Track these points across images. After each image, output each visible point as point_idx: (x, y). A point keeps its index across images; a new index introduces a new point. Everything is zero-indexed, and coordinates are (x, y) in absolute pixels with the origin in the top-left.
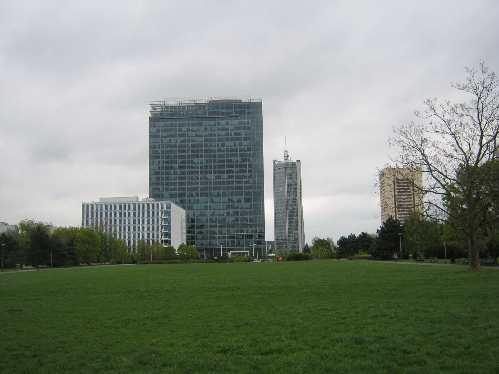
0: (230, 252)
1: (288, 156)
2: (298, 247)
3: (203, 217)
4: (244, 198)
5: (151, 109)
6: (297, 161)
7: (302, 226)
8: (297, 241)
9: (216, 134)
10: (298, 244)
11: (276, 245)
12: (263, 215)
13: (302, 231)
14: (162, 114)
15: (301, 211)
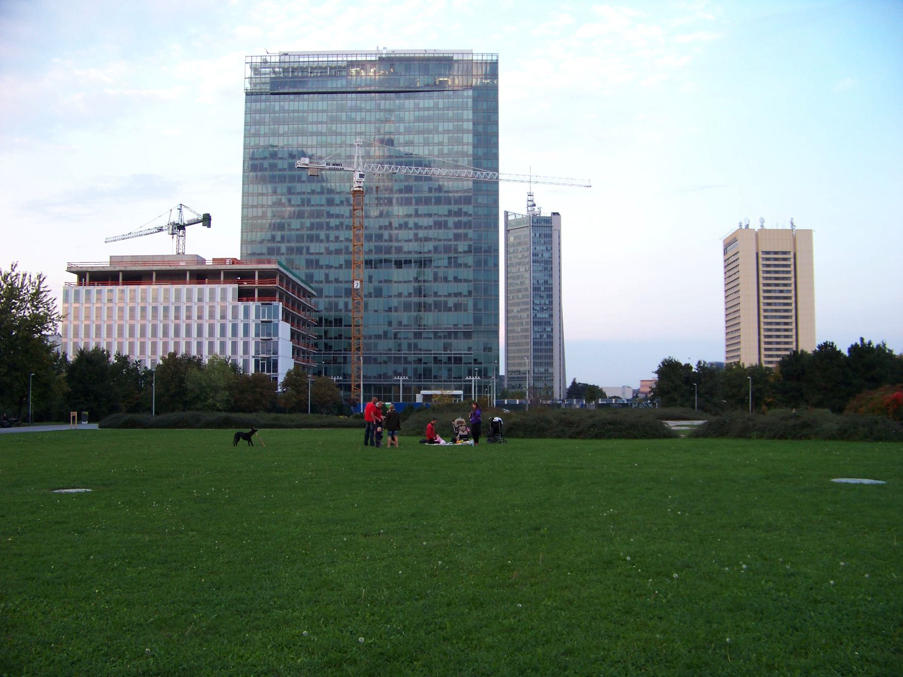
0: (420, 393)
1: (534, 205)
2: (552, 350)
3: (370, 299)
4: (444, 344)
5: (249, 73)
6: (554, 214)
8: (551, 361)
9: (371, 336)
12: (494, 150)
14: (274, 82)
15: (560, 314)
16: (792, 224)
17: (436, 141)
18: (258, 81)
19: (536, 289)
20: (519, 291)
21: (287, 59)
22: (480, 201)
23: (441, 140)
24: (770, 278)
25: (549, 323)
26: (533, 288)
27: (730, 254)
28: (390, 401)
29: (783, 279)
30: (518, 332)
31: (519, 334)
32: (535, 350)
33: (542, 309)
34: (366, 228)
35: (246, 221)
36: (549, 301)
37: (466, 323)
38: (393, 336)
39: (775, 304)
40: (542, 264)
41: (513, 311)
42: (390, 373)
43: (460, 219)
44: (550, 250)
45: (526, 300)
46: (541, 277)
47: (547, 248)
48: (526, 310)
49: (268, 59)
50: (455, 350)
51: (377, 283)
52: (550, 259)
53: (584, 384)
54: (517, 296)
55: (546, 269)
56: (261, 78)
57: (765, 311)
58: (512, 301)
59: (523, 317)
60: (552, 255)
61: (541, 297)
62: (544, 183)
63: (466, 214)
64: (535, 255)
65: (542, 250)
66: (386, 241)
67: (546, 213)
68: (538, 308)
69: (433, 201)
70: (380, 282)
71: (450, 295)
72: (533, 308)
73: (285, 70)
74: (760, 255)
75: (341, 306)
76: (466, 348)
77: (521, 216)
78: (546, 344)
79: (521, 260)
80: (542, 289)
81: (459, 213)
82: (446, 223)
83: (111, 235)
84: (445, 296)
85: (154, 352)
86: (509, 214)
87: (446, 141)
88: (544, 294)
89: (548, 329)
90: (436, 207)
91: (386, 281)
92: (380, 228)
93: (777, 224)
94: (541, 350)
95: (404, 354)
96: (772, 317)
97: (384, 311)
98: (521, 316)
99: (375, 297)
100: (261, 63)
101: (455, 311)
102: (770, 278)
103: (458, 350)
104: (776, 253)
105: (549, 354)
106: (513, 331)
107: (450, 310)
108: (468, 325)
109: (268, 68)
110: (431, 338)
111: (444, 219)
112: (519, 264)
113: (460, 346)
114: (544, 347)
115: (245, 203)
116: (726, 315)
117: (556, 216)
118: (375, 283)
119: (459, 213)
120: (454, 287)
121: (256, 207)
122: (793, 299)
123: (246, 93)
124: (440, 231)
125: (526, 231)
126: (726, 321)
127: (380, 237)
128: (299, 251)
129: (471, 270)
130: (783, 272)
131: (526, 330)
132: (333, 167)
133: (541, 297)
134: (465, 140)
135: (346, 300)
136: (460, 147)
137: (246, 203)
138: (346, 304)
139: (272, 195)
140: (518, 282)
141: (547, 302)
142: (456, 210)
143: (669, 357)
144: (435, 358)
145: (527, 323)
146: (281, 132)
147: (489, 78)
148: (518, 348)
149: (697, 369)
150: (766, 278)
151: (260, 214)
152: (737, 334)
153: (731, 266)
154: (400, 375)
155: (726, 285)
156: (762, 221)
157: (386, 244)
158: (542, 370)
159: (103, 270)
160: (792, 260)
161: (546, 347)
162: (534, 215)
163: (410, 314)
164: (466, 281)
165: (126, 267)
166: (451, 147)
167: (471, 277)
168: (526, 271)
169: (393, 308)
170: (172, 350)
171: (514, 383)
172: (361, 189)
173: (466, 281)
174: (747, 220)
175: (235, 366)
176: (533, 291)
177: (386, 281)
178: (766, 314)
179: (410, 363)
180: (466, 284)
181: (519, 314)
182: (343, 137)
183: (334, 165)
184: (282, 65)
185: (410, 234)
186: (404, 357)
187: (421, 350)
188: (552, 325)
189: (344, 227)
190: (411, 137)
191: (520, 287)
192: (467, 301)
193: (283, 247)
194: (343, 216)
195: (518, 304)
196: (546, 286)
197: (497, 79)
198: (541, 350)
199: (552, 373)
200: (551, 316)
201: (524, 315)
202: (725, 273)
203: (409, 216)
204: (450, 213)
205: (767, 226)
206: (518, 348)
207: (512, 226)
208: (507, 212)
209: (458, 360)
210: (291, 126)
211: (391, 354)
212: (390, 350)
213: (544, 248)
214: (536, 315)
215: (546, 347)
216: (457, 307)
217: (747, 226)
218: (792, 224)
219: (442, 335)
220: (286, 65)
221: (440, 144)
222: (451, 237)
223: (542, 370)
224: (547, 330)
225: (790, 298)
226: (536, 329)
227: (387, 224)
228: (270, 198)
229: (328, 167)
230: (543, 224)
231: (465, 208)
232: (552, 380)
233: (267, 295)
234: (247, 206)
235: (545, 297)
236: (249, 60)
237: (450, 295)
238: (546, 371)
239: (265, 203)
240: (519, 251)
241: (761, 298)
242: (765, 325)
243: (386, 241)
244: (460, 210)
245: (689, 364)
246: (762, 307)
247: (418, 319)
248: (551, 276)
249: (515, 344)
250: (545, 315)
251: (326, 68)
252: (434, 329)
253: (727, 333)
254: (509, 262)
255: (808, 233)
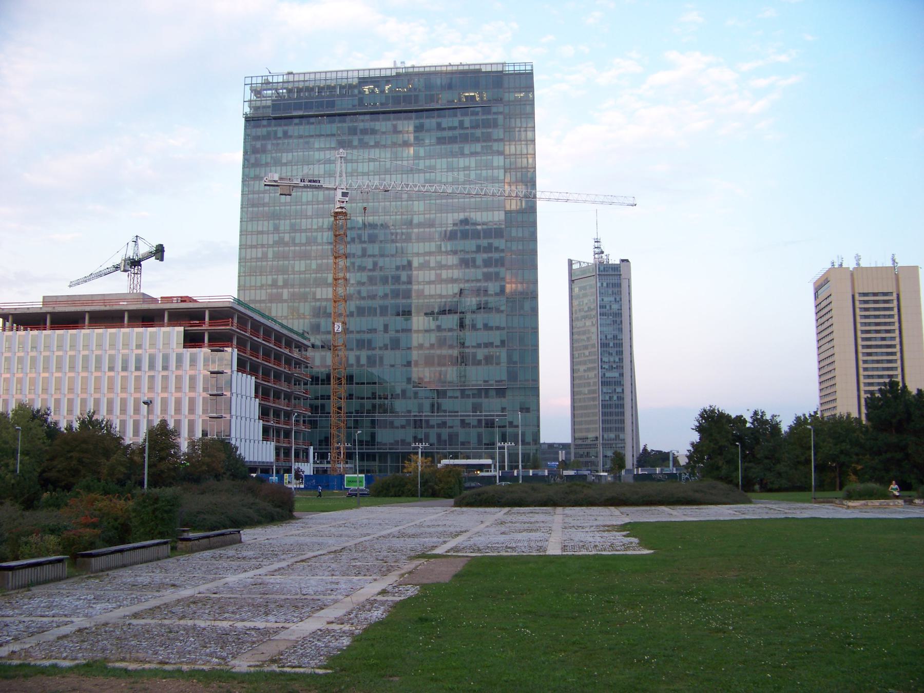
1: (602, 252)
2: (623, 414)
4: (473, 404)
5: (249, 95)
6: (623, 261)
7: (632, 407)
8: (622, 410)
10: (624, 416)
11: (575, 449)
13: (634, 428)
14: (275, 106)
16: (894, 261)
17: (461, 165)
18: (258, 104)
19: (604, 345)
20: (586, 347)
21: (291, 78)
22: (514, 234)
23: (467, 164)
24: (869, 324)
25: (620, 383)
26: (601, 344)
27: (821, 298)
28: (364, 473)
29: (885, 324)
30: (585, 394)
31: (586, 396)
32: (604, 414)
33: (612, 368)
34: (381, 269)
35: (243, 264)
36: (619, 359)
37: (498, 379)
38: (412, 395)
39: (876, 354)
40: (610, 317)
41: (579, 370)
42: (410, 439)
43: (490, 255)
44: (618, 301)
45: (593, 357)
46: (610, 331)
47: (615, 299)
48: (594, 368)
49: (270, 79)
50: (486, 411)
51: (393, 333)
52: (620, 311)
53: (657, 451)
54: (584, 354)
55: (615, 322)
56: (261, 100)
57: (865, 362)
58: (577, 360)
59: (590, 376)
60: (621, 306)
61: (611, 354)
62: (576, 201)
63: (497, 249)
64: (602, 307)
65: (611, 302)
66: (404, 283)
67: (615, 260)
68: (606, 366)
69: (459, 235)
70: (397, 331)
71: (479, 346)
72: (602, 367)
73: (290, 91)
74: (857, 297)
75: (352, 360)
76: (500, 409)
77: (586, 264)
78: (617, 406)
79: (588, 313)
80: (611, 344)
81: (489, 249)
82: (474, 260)
83: (74, 279)
84: (473, 347)
85: (70, 411)
86: (573, 262)
87: (473, 165)
88: (613, 351)
89: (619, 390)
90: (462, 242)
91: (403, 331)
92: (398, 268)
93: (876, 262)
94: (611, 414)
95: (426, 416)
96: (873, 369)
97: (402, 365)
98: (588, 375)
99: (392, 349)
100: (262, 84)
101: (487, 364)
102: (869, 324)
103: (489, 411)
104: (875, 294)
105: (619, 418)
106: (580, 393)
107: (479, 363)
108: (501, 381)
109: (269, 90)
110: (457, 397)
111: (472, 256)
112: (585, 317)
113: (492, 406)
114: (613, 410)
115: (242, 243)
116: (820, 369)
117: (625, 263)
118: (392, 333)
119: (489, 249)
120: (484, 336)
121: (256, 247)
122: (898, 347)
123: (246, 118)
124: (467, 270)
125: (592, 281)
126: (820, 383)
127: (397, 279)
128: (303, 298)
129: (504, 316)
130: (885, 316)
131: (594, 392)
132: (309, 184)
133: (611, 354)
134: (495, 164)
135: (358, 353)
136: (490, 172)
137: (245, 243)
138: (358, 359)
139: (273, 233)
140: (584, 337)
141: (617, 360)
142: (486, 245)
143: (711, 407)
144: (463, 421)
145: (595, 383)
146: (284, 161)
147: (524, 92)
148: (585, 412)
149: (752, 423)
150: (865, 324)
151: (260, 255)
152: (832, 390)
153: (823, 311)
154: (421, 441)
155: (818, 333)
156: (858, 258)
157: (404, 287)
158: (612, 435)
159: (30, 311)
160: (895, 302)
161: (617, 410)
162: (600, 262)
163: (432, 369)
164: (498, 328)
165: (54, 307)
166: (479, 172)
167: (503, 325)
168: (593, 325)
169: (413, 363)
170: (91, 407)
171: (581, 451)
172: (344, 210)
173: (498, 328)
174: (840, 258)
175: (109, 426)
176: (601, 347)
177: (403, 331)
178: (866, 366)
179: (433, 427)
180: (498, 332)
181: (586, 374)
182: (354, 165)
183: (310, 181)
184: (286, 85)
185: (432, 275)
186: (425, 420)
187: (445, 411)
188: (623, 385)
189: (356, 268)
190: (433, 161)
191: (587, 343)
192: (500, 352)
193: (286, 293)
194: (354, 255)
195: (585, 363)
196: (615, 341)
197: (533, 92)
198: (611, 414)
199: (624, 440)
200: (622, 375)
201: (592, 374)
202: (817, 320)
203: (430, 253)
204: (479, 249)
205: (864, 264)
206: (585, 412)
207: (577, 276)
208: (571, 261)
209: (490, 424)
210: (295, 154)
211: (410, 416)
212: (409, 412)
213: (612, 299)
214: (604, 374)
215: (617, 410)
216: (488, 360)
217: (841, 265)
218: (894, 261)
219: (470, 393)
220: (290, 86)
221: (467, 168)
222: (480, 277)
223: (612, 435)
224: (617, 391)
225: (894, 346)
226: (605, 390)
227: (405, 263)
228: (271, 236)
229: (302, 184)
230: (611, 273)
231: (496, 242)
232: (624, 447)
233: (219, 341)
234: (245, 247)
235: (614, 354)
236: (248, 81)
237: (479, 346)
238: (617, 437)
239: (265, 242)
240: (585, 303)
241: (860, 348)
242: (864, 379)
243: (404, 283)
244: (490, 245)
245: (742, 416)
246: (861, 357)
247: (462, 376)
248: (621, 330)
249: (582, 408)
250: (615, 374)
251: (334, 87)
252: (461, 386)
253: (821, 390)
254: (574, 316)
255: (914, 270)
